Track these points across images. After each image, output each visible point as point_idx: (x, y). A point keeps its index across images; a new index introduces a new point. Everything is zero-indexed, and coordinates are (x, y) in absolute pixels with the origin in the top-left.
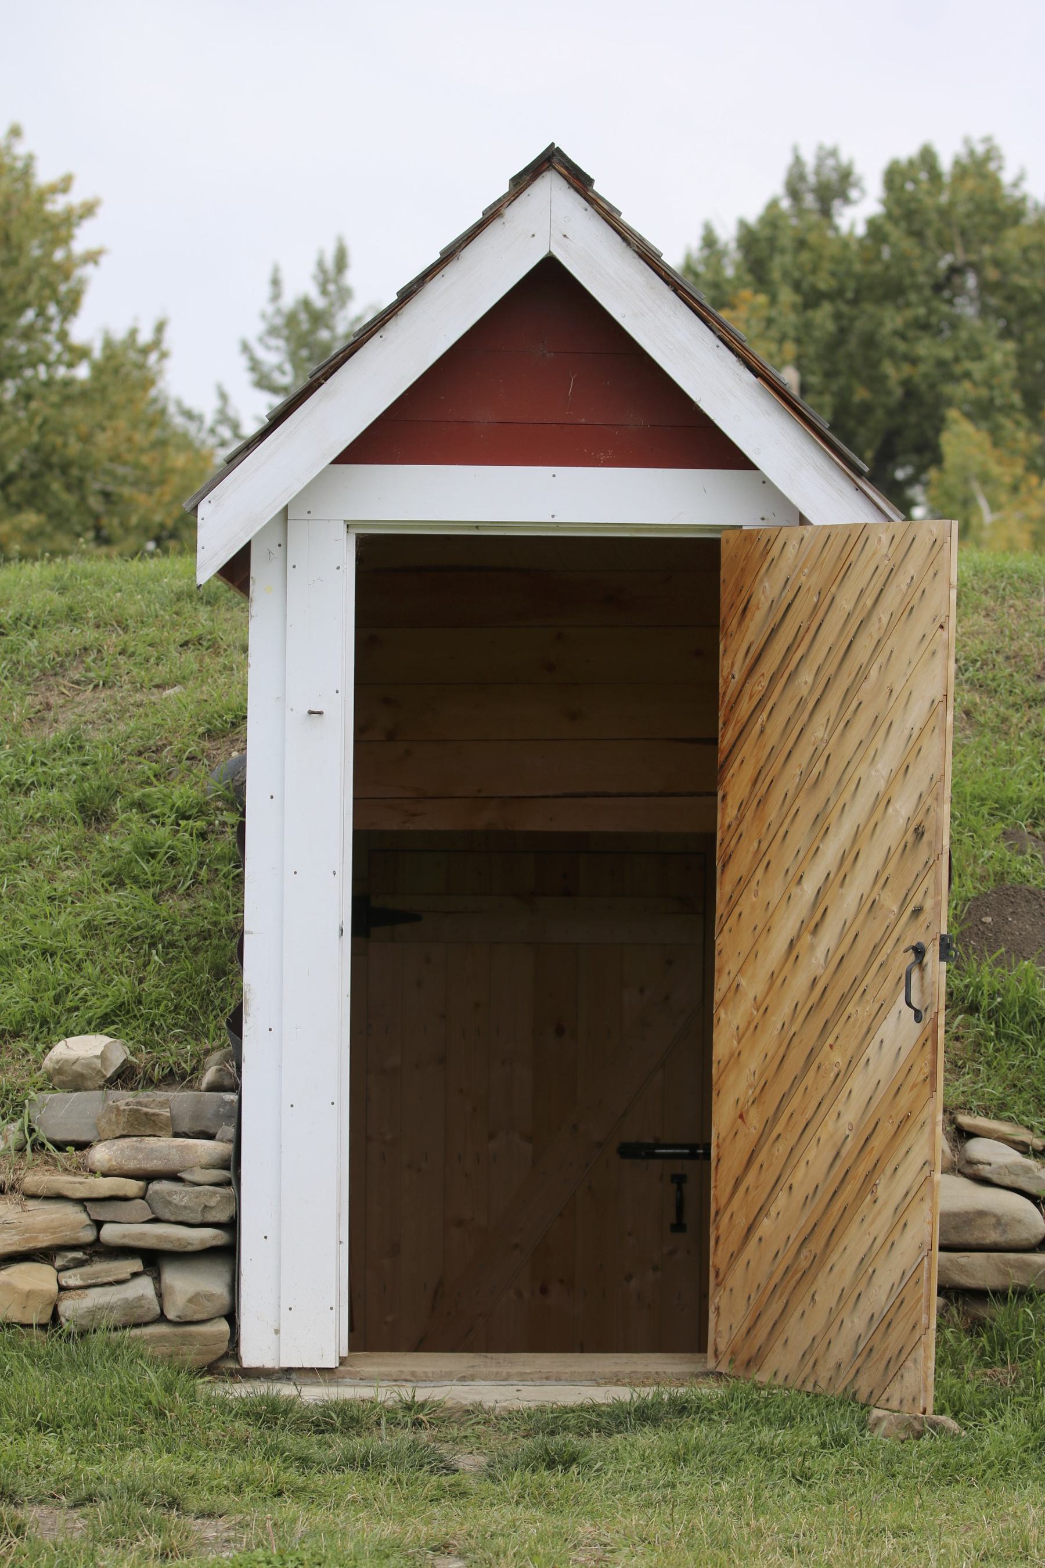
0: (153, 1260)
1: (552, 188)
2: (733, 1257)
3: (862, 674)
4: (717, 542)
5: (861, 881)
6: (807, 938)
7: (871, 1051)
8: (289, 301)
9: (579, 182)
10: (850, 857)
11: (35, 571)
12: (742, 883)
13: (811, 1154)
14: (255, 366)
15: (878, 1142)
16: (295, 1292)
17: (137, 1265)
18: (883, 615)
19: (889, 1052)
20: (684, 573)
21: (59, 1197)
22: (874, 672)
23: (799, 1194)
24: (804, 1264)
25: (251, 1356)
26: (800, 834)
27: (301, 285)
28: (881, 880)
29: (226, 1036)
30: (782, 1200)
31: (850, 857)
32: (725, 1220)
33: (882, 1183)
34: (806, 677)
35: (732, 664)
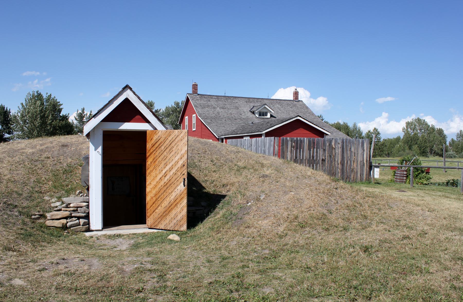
0: (79, 218)
1: (129, 91)
2: (151, 215)
3: (173, 147)
4: (146, 132)
5: (174, 171)
6: (163, 177)
7: (176, 190)
9: (131, 89)
10: (171, 168)
12: (151, 171)
13: (165, 202)
15: (178, 201)
17: (76, 219)
18: (176, 140)
19: (179, 190)
20: (143, 134)
21: (67, 211)
22: (175, 147)
23: (163, 207)
24: (164, 214)
25: (92, 228)
26: (162, 165)
28: (177, 171)
29: (86, 191)
30: (160, 208)
31: (171, 168)
32: (149, 210)
33: (178, 205)
34: (163, 147)
35: (149, 146)
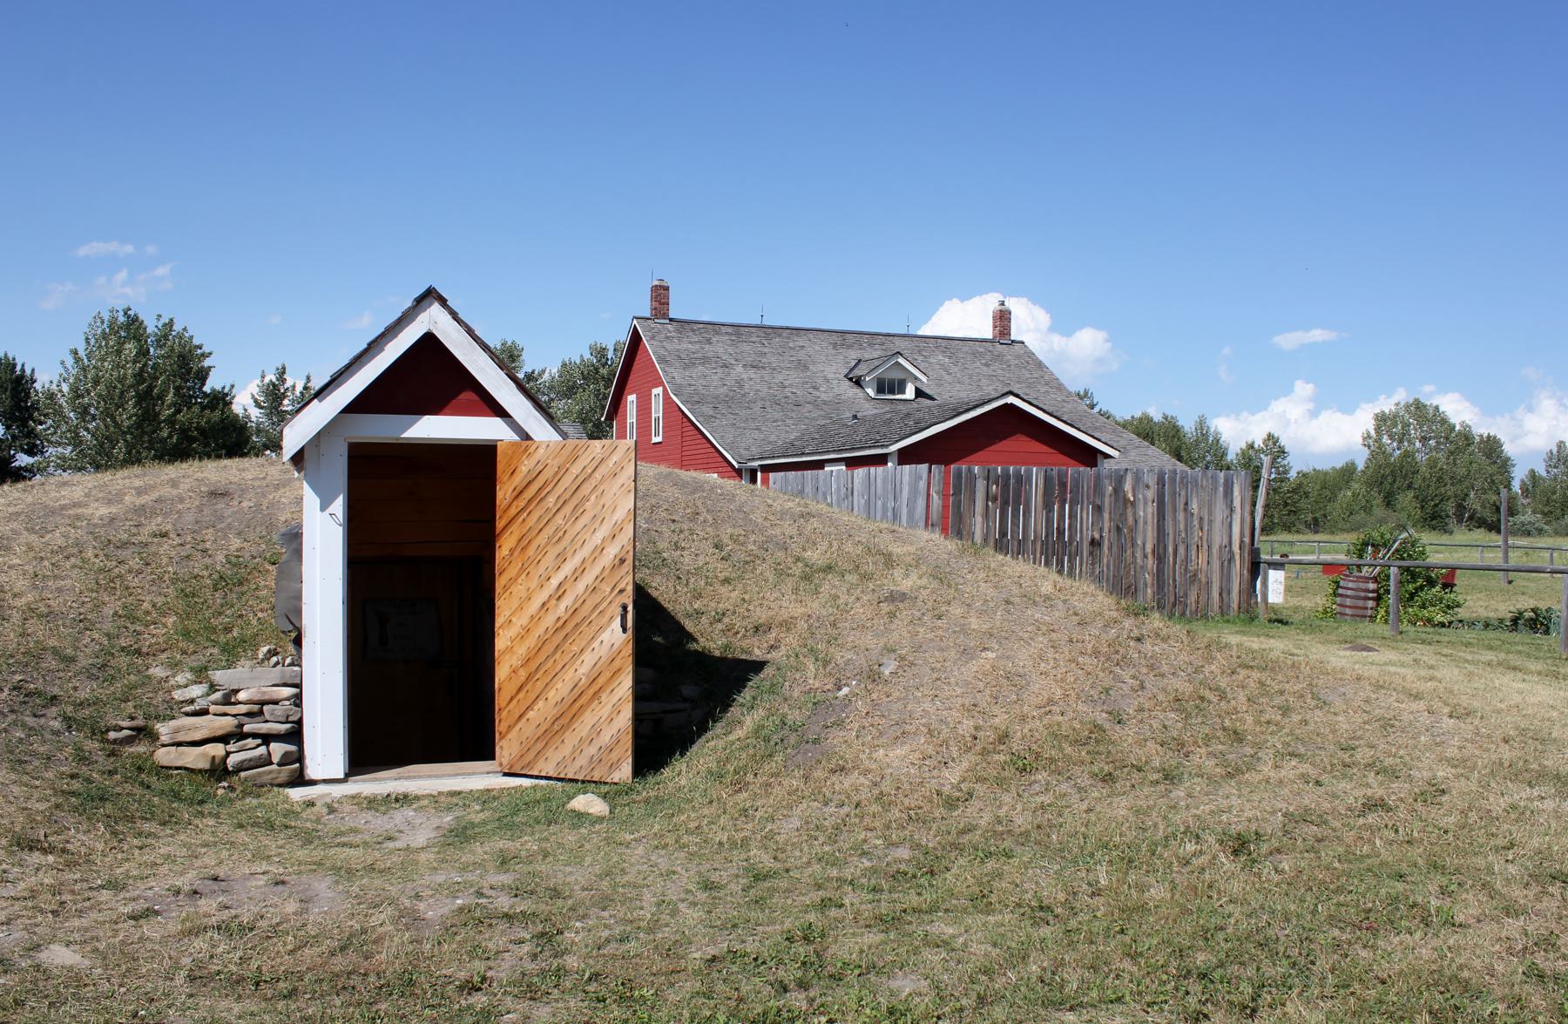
0: (267, 739)
1: (436, 308)
3: (586, 499)
4: (495, 447)
5: (588, 579)
6: (553, 602)
7: (596, 644)
8: (267, 380)
9: (443, 302)
10: (580, 571)
11: (89, 481)
12: (513, 580)
13: (559, 685)
14: (256, 401)
15: (601, 680)
16: (326, 745)
17: (259, 741)
18: (598, 475)
19: (606, 646)
21: (225, 714)
22: (593, 498)
23: (552, 702)
24: (556, 727)
25: (312, 772)
26: (549, 560)
27: (271, 377)
28: (600, 579)
29: (291, 648)
30: (540, 704)
31: (580, 571)
33: (604, 696)
34: (551, 499)
35: (503, 493)
